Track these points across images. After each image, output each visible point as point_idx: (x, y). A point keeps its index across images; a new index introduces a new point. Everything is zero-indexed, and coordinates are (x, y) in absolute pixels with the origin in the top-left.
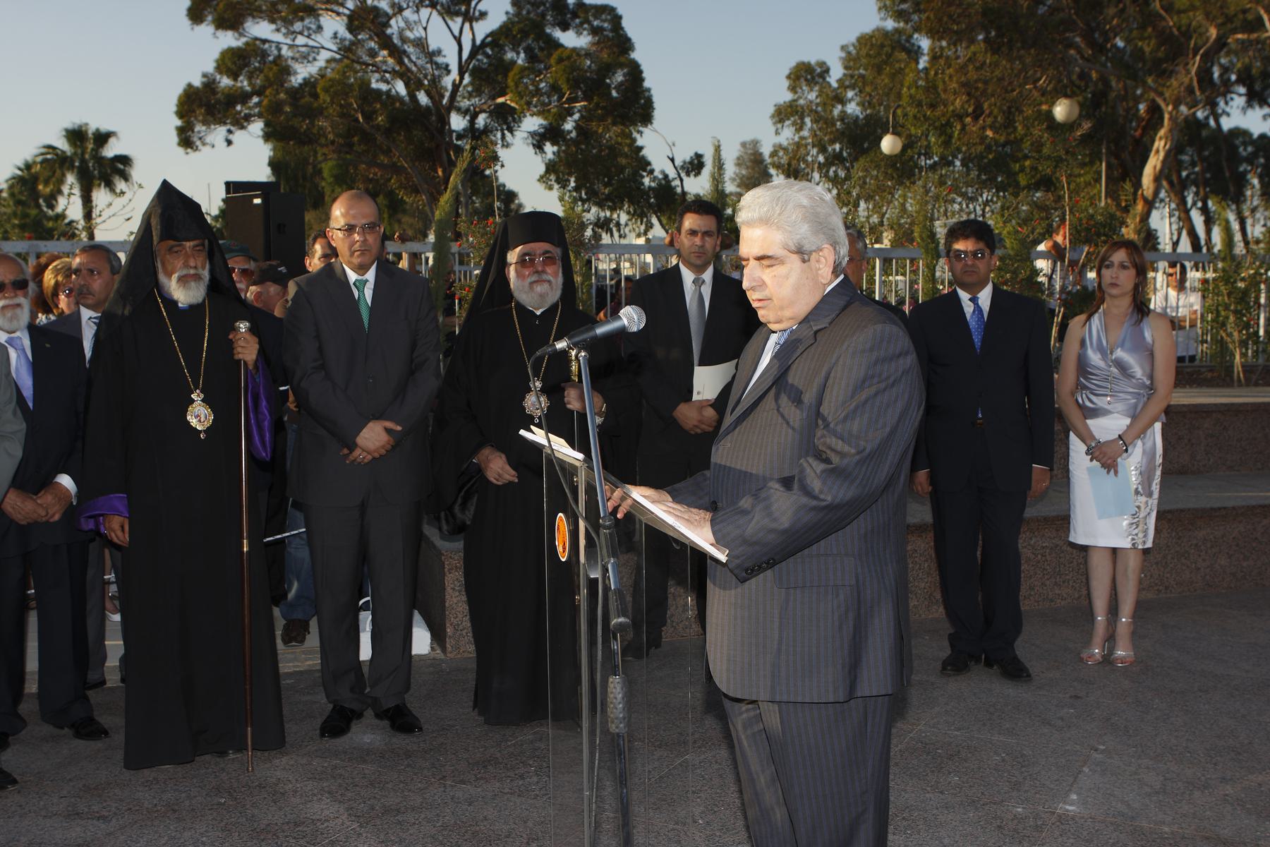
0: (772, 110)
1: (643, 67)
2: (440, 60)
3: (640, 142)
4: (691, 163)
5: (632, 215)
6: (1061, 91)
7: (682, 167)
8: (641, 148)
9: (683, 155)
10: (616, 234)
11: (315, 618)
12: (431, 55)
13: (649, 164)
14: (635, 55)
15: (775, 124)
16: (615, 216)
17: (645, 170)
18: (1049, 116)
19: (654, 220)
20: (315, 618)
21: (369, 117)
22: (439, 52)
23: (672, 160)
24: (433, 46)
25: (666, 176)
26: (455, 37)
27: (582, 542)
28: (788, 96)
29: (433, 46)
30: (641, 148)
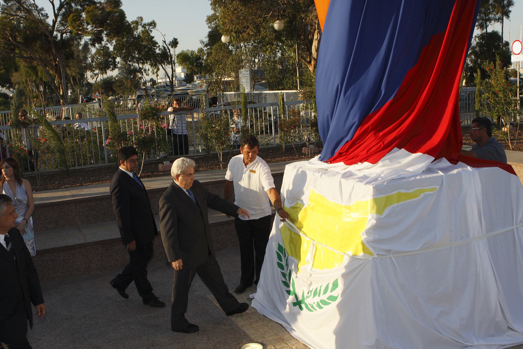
0: (206, 18)
1: (126, 13)
2: (43, 12)
3: (152, 34)
4: (173, 42)
5: (151, 65)
6: (274, 18)
7: (169, 45)
8: (153, 37)
9: (169, 40)
10: (144, 74)
11: (133, 284)
12: (40, 11)
13: (157, 43)
14: (122, 8)
15: (208, 24)
16: (144, 66)
17: (156, 46)
18: (273, 27)
19: (160, 67)
20: (133, 284)
21: (15, 38)
22: (42, 9)
23: (165, 42)
24: (40, 7)
25: (164, 48)
26: (50, 2)
27: (494, 268)
28: (212, 12)
29: (40, 7)
30: (153, 37)
